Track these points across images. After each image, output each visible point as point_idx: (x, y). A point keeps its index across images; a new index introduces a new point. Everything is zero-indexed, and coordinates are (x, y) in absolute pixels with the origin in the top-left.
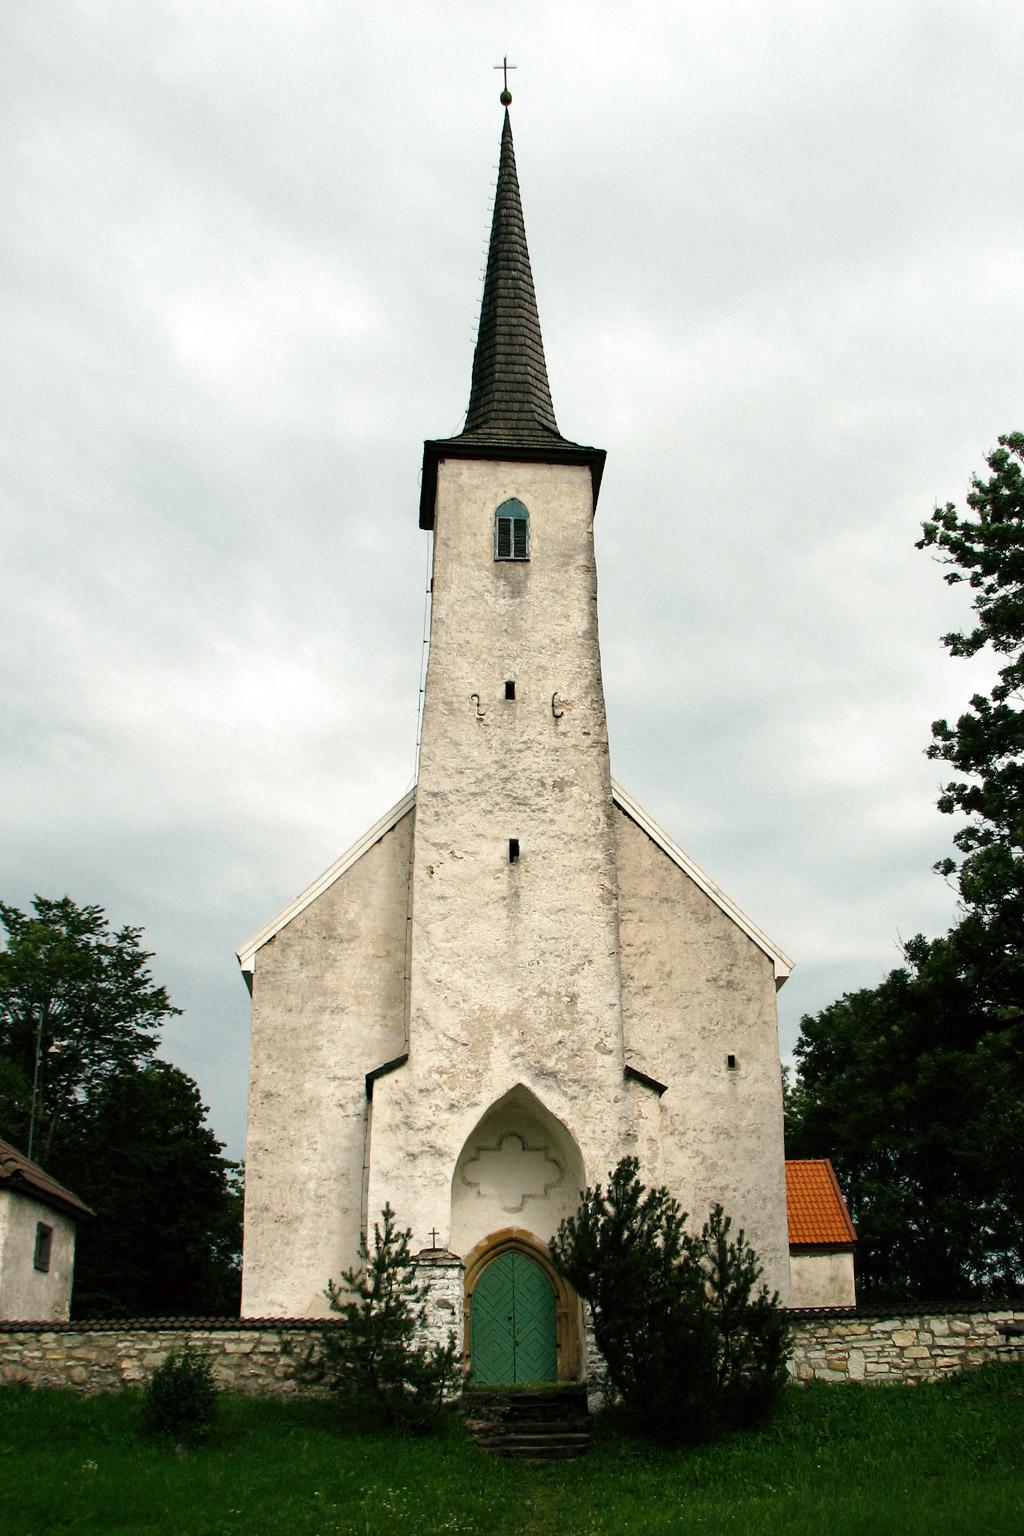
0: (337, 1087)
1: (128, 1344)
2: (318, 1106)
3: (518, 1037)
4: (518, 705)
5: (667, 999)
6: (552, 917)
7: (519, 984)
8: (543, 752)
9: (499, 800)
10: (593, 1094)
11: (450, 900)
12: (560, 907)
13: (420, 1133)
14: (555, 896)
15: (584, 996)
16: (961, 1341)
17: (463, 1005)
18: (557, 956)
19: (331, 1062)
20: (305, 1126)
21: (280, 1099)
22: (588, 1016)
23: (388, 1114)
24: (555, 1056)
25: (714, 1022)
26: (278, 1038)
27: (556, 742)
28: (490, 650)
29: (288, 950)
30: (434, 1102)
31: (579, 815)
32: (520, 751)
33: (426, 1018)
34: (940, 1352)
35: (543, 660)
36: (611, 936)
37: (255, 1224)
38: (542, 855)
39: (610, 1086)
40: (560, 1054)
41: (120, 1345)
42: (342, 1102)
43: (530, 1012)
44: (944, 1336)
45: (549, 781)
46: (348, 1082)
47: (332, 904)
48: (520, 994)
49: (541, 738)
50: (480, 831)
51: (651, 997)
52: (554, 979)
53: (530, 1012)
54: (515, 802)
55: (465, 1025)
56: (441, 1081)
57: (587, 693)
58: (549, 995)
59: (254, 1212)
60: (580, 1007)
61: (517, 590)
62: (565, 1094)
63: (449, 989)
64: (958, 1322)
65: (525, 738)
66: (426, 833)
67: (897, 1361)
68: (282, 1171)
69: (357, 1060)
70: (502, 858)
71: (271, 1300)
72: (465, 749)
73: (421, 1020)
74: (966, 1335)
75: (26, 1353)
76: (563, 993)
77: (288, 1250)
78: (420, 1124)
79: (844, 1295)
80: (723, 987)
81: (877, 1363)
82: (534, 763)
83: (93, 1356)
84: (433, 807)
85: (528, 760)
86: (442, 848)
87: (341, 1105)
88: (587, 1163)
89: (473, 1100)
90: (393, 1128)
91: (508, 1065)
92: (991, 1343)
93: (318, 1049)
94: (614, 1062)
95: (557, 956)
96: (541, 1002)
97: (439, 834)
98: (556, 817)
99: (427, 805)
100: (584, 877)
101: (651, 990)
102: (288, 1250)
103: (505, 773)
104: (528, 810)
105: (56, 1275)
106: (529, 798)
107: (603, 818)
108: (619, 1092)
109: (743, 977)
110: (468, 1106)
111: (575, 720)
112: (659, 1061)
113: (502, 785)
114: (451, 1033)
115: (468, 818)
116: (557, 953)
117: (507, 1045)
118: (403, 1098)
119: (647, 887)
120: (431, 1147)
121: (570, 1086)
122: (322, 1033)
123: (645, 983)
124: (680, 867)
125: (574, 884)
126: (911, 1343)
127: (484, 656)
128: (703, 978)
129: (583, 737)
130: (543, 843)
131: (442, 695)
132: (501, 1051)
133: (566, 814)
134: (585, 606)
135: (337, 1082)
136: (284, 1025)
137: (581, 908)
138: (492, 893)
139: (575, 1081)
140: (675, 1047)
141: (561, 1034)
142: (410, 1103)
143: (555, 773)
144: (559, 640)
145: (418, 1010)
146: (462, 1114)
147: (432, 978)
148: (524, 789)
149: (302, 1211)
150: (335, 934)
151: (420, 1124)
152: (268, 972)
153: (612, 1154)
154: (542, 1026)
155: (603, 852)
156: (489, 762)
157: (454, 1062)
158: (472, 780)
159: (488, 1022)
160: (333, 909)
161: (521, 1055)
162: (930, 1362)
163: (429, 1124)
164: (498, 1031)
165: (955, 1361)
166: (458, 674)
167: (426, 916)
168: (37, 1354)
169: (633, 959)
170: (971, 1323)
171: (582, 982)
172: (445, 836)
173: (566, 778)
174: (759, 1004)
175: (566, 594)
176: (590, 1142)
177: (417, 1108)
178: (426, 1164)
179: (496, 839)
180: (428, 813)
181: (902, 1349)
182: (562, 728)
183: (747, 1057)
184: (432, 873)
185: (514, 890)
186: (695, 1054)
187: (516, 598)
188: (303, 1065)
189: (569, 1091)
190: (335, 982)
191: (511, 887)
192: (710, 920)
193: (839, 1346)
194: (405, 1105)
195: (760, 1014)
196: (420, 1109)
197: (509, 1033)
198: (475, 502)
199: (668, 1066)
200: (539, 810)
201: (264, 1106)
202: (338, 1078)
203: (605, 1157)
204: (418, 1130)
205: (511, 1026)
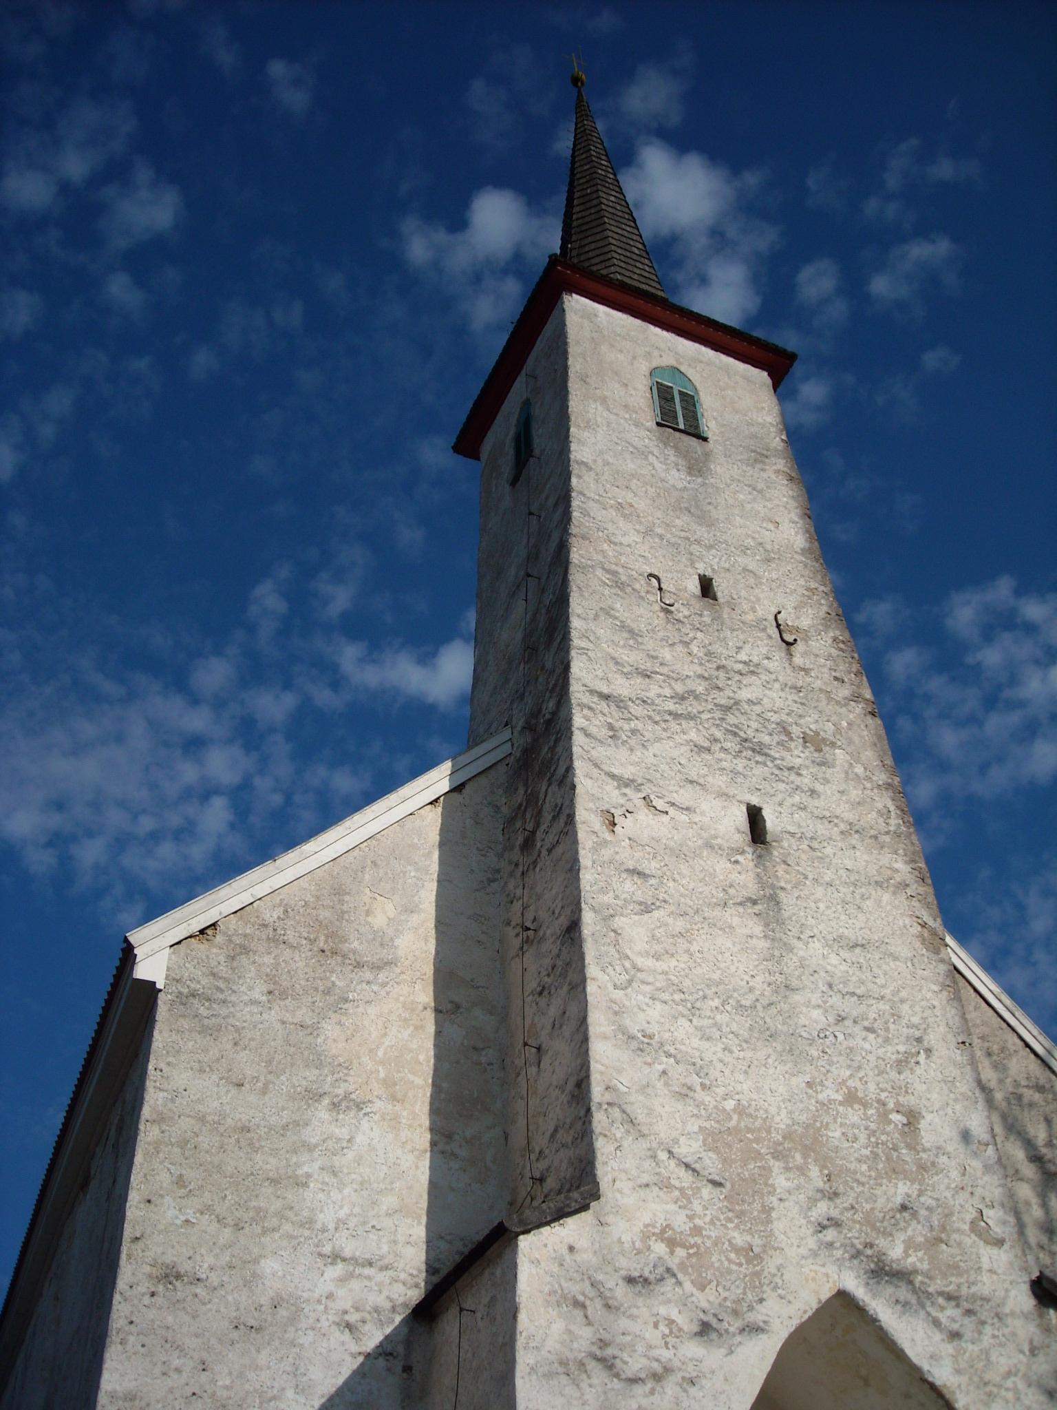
0: (342, 1280)
2: (293, 1320)
3: (821, 1184)
9: (719, 734)
10: (988, 1330)
13: (639, 1390)
15: (929, 1117)
17: (700, 1095)
22: (943, 1159)
23: (558, 1327)
24: (900, 1237)
26: (205, 1140)
29: (244, 960)
33: (628, 1109)
40: (910, 1232)
42: (353, 1318)
46: (367, 1271)
55: (713, 1140)
56: (673, 1263)
58: (865, 1105)
62: (936, 1323)
63: (669, 1055)
65: (743, 656)
66: (593, 752)
69: (387, 1223)
70: (739, 832)
73: (616, 1113)
78: (635, 1364)
86: (627, 786)
87: (349, 1326)
89: (752, 1317)
94: (1011, 1263)
95: (867, 1029)
97: (623, 761)
100: (886, 897)
106: (769, 747)
110: (742, 1331)
116: (866, 1023)
118: (591, 1292)
121: (942, 1309)
122: (311, 1148)
125: (869, 903)
135: (339, 1269)
138: (731, 886)
141: (902, 1190)
142: (608, 1306)
143: (802, 721)
146: (731, 1352)
151: (635, 1364)
152: (193, 995)
154: (864, 1167)
157: (698, 1222)
159: (757, 1141)
160: (341, 902)
161: (836, 1223)
163: (659, 1370)
164: (781, 1164)
177: (624, 1323)
182: (798, 660)
188: (260, 1215)
189: (943, 1317)
197: (802, 1170)
201: (158, 1300)
202: (344, 1260)
204: (634, 1381)
205: (805, 1157)
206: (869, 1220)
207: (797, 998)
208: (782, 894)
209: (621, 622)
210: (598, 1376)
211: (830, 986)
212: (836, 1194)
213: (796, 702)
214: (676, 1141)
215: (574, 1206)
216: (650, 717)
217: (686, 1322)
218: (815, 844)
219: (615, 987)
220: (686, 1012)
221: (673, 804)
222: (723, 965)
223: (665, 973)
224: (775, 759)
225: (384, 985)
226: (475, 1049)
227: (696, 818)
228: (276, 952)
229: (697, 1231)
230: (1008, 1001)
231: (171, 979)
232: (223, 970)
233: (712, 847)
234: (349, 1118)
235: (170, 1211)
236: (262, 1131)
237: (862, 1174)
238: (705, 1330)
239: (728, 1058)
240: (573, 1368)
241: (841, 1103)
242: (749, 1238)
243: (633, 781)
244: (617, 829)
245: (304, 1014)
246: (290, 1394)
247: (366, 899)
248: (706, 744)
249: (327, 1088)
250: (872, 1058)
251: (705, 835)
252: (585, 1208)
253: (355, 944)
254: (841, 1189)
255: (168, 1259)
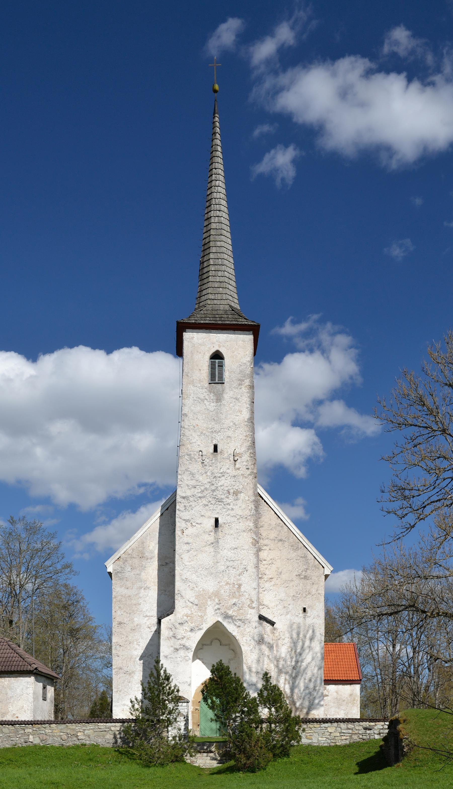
1: (80, 728)
2: (140, 628)
3: (217, 602)
4: (219, 456)
5: (279, 583)
6: (232, 551)
7: (219, 580)
8: (230, 477)
9: (210, 499)
11: (191, 544)
12: (235, 547)
13: (179, 640)
14: (234, 542)
15: (244, 585)
16: (350, 731)
17: (196, 589)
18: (233, 568)
19: (144, 610)
20: (135, 636)
21: (125, 625)
22: (245, 593)
23: (167, 632)
25: (298, 593)
26: (123, 600)
27: (234, 473)
28: (207, 428)
29: (126, 563)
30: (185, 628)
31: (244, 506)
32: (220, 477)
33: (181, 594)
34: (343, 735)
35: (230, 433)
36: (256, 560)
37: (117, 674)
38: (228, 524)
39: (253, 622)
40: (234, 609)
41: (77, 728)
42: (149, 626)
43: (222, 591)
44: (345, 729)
45: (232, 491)
46: (152, 618)
47: (143, 543)
48: (218, 584)
49: (228, 471)
50: (203, 514)
51: (273, 583)
52: (232, 577)
53: (222, 591)
54: (217, 501)
55: (197, 597)
57: (248, 449)
58: (230, 584)
59: (116, 670)
60: (242, 589)
61: (219, 399)
62: (235, 625)
63: (190, 582)
64: (350, 725)
65: (222, 471)
67: (329, 737)
68: (126, 653)
71: (124, 704)
72: (197, 476)
74: (352, 729)
75: (46, 731)
76: (236, 584)
77: (130, 684)
78: (179, 637)
79: (355, 702)
80: (302, 578)
81: (322, 737)
82: (225, 482)
83: (68, 731)
84: (183, 503)
85: (223, 481)
86: (187, 521)
87: (149, 627)
88: (244, 653)
90: (169, 638)
91: (213, 613)
92: (360, 732)
93: (140, 604)
95: (233, 568)
96: (227, 587)
98: (234, 507)
99: (181, 502)
100: (245, 534)
101: (273, 579)
102: (130, 684)
103: (213, 488)
104: (222, 504)
105: (49, 701)
107: (253, 507)
108: (257, 624)
109: (312, 574)
111: (243, 462)
112: (275, 609)
113: (212, 493)
114: (191, 600)
115: (198, 508)
116: (234, 567)
117: (213, 605)
119: (273, 535)
120: (184, 646)
121: (237, 622)
122: (140, 597)
123: (270, 577)
124: (287, 526)
126: (333, 731)
127: (204, 432)
128: (295, 574)
129: (246, 470)
130: (229, 519)
131: (187, 451)
132: (211, 607)
133: (239, 506)
134: (248, 406)
135: (147, 618)
136: (126, 594)
137: (243, 547)
138: (208, 541)
139: (240, 620)
140: (282, 604)
141: (234, 600)
142: (175, 628)
144: (237, 423)
145: (178, 591)
147: (184, 578)
148: (221, 495)
149: (135, 669)
150: (145, 555)
151: (179, 637)
152: (118, 572)
153: (253, 649)
155: (253, 523)
156: (206, 482)
157: (192, 612)
158: (200, 491)
160: (144, 545)
161: (219, 609)
162: (340, 738)
164: (210, 600)
165: (348, 738)
166: (193, 441)
167: (181, 551)
168: (50, 731)
169: (266, 566)
170: (354, 725)
171: (243, 579)
172: (189, 516)
173: (239, 490)
174: (317, 586)
175: (240, 400)
176: (245, 644)
177: (178, 631)
178: (182, 653)
179: (209, 517)
180: (181, 506)
181: (331, 733)
182: (237, 466)
183: (311, 608)
184: (183, 532)
185: (216, 540)
186: (290, 606)
187: (218, 402)
189: (237, 624)
190: (145, 576)
191: (215, 538)
192: (299, 549)
193: (310, 731)
194: (173, 629)
195: (317, 590)
196: (180, 631)
197: (214, 600)
198: (200, 353)
199: (279, 612)
200: (227, 504)
203: (251, 650)
206: (226, 608)
207: (219, 564)
208: (219, 540)
209: (190, 472)
210: (173, 639)
211: (227, 560)
212: (220, 603)
213: (233, 481)
214: (190, 599)
215: (170, 613)
216: (194, 500)
217: (188, 629)
218: (230, 524)
219: (181, 570)
220: (195, 572)
221: (197, 523)
222: (203, 560)
223: (191, 565)
224: (224, 502)
225: (152, 562)
226: (170, 572)
227: (202, 525)
228: (132, 560)
229: (192, 613)
230: (301, 534)
231: (114, 570)
232: (123, 566)
233: (205, 532)
234: (147, 591)
235: (119, 613)
236: (133, 596)
237: (227, 599)
238: (192, 630)
239: (202, 580)
240: (169, 638)
241: (225, 585)
242: (201, 614)
243: (188, 520)
244: (184, 534)
245: (138, 572)
246: (140, 639)
247: (148, 543)
248: (207, 503)
249: (143, 586)
250: (233, 574)
251: (203, 529)
252: (172, 613)
253: (147, 554)
254: (222, 602)
255: (120, 621)
